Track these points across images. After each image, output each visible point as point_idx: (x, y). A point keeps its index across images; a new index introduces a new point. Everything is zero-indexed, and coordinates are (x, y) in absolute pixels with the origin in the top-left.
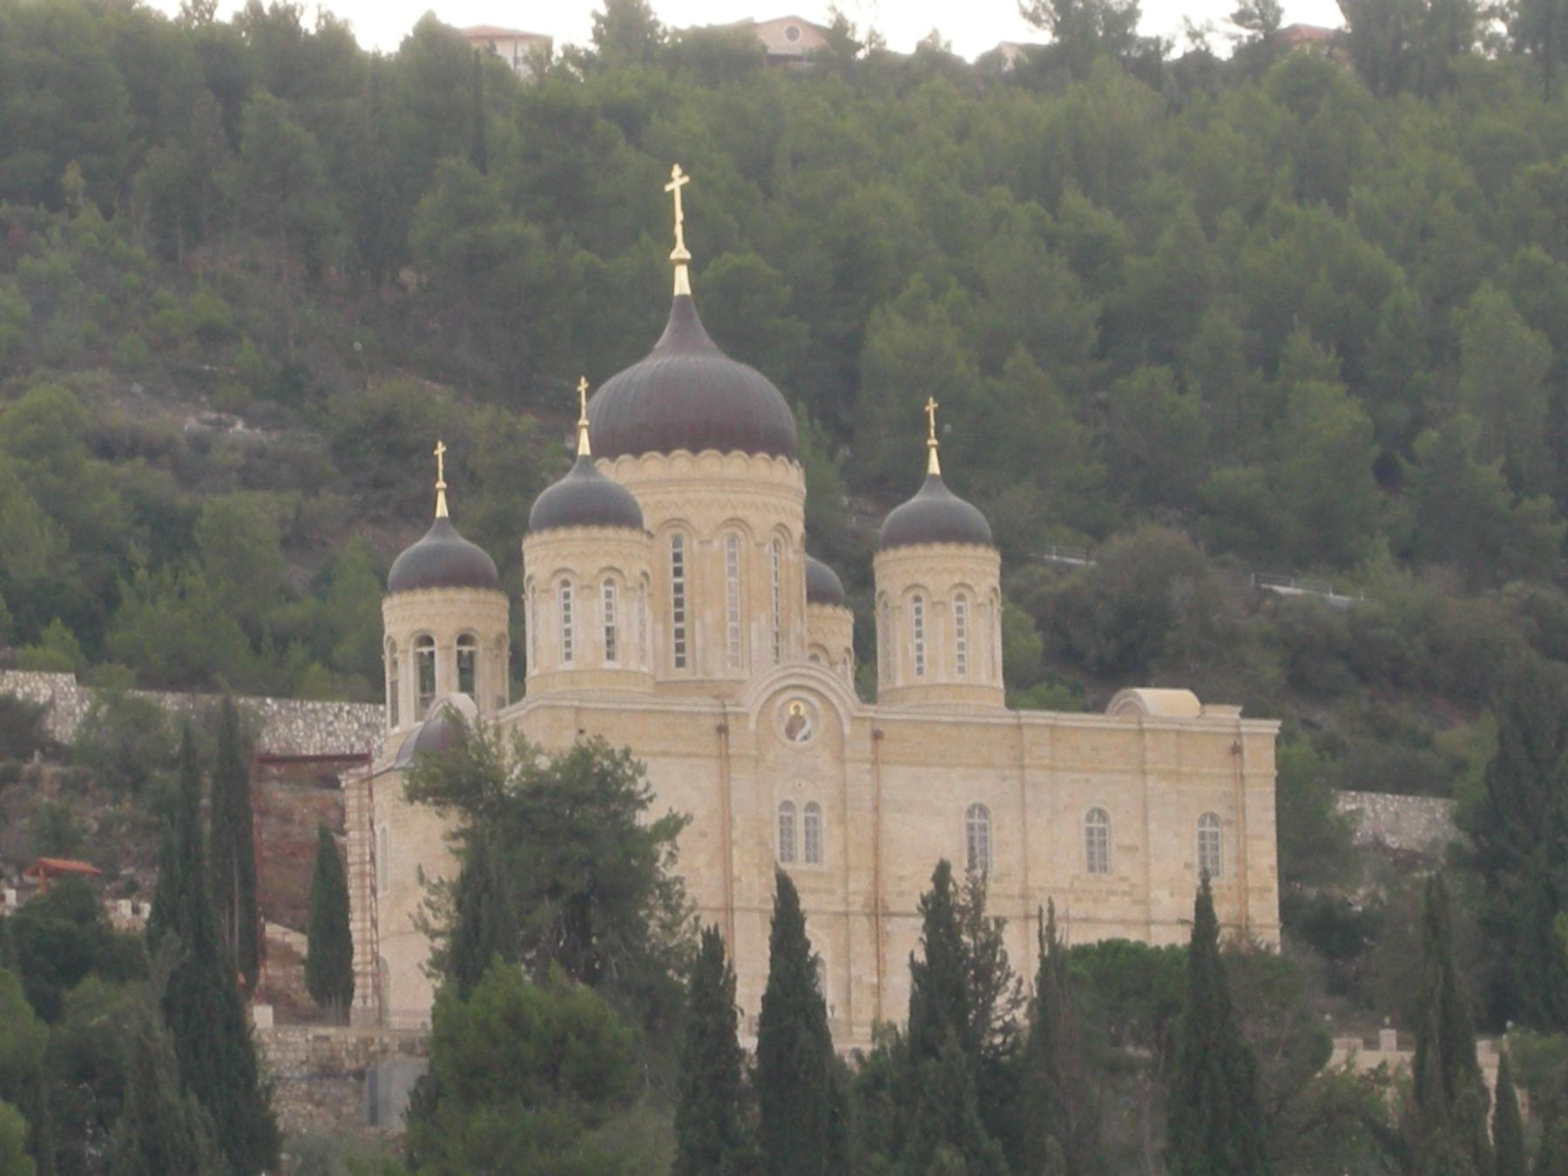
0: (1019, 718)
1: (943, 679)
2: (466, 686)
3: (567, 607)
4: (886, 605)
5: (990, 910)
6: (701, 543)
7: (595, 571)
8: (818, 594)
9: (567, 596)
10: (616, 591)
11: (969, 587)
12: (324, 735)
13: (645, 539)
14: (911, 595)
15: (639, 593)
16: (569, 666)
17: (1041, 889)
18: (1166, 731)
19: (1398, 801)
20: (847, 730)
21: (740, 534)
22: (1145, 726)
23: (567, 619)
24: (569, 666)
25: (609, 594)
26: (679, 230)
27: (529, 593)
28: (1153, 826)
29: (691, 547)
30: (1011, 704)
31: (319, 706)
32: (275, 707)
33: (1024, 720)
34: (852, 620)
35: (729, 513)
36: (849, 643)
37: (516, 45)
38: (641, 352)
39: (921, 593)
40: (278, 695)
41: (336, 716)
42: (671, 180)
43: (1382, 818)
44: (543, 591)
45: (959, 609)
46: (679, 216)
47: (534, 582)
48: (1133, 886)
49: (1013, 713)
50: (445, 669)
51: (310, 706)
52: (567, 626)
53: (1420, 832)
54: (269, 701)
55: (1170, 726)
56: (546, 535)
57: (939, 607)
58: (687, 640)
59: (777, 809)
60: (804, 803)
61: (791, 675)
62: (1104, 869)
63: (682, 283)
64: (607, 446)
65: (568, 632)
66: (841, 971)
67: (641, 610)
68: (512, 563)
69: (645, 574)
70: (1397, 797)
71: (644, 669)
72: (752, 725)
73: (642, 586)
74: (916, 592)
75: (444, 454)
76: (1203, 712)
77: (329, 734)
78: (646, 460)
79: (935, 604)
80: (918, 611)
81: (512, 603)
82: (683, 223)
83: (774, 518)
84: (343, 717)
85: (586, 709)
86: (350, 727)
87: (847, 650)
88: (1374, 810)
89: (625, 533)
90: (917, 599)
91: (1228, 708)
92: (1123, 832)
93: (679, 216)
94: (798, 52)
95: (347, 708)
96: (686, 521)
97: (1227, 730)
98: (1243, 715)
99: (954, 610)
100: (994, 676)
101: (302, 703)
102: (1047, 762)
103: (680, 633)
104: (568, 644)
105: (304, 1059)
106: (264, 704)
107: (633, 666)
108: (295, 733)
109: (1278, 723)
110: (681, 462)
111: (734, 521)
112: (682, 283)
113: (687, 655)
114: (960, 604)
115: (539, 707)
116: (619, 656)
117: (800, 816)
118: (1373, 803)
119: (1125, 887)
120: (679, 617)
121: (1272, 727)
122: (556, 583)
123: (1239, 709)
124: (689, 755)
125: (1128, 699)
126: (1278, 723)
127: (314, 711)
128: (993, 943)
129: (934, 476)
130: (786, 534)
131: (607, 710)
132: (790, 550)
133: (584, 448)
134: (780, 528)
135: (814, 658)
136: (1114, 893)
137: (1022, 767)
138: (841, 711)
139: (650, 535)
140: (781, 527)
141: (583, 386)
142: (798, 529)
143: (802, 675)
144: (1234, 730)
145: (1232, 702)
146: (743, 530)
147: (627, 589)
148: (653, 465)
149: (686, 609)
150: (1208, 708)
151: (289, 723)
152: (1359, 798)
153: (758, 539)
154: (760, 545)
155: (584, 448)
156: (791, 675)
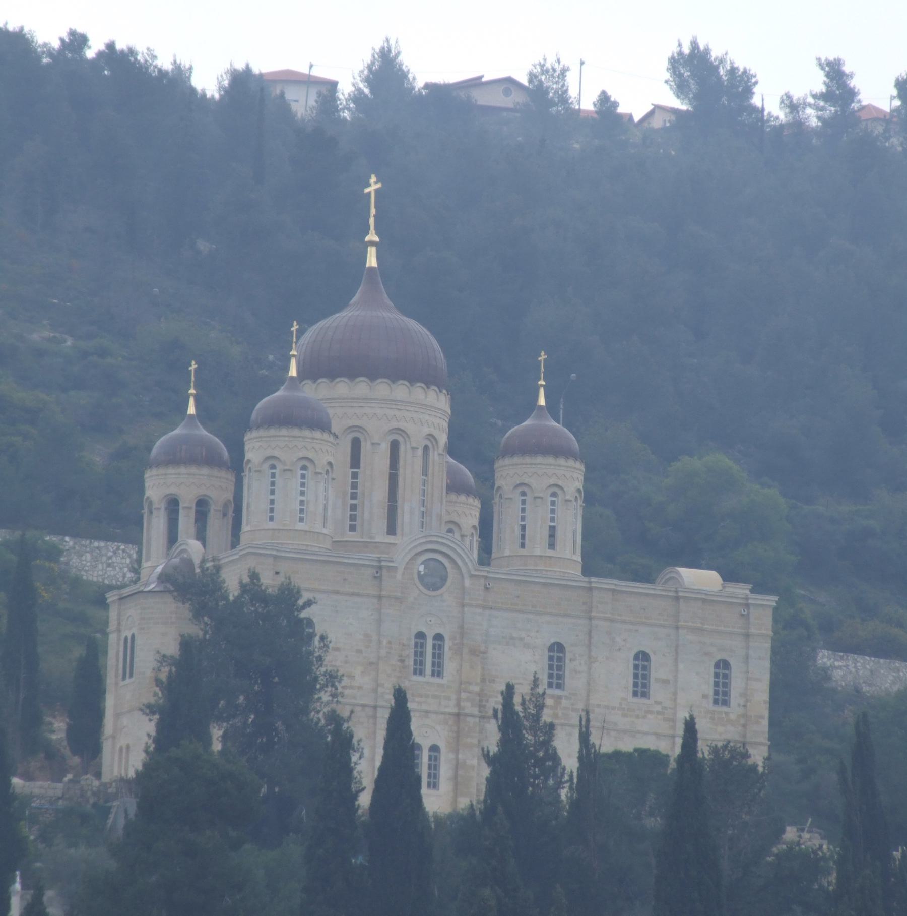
0: (590, 582)
1: (538, 552)
2: (201, 536)
3: (273, 484)
4: (501, 496)
5: (546, 717)
6: (373, 444)
7: (295, 459)
8: (455, 487)
9: (273, 476)
10: (309, 474)
11: (526, 485)
12: (105, 565)
13: (331, 439)
14: (520, 490)
15: (326, 477)
16: (271, 525)
17: (598, 706)
18: (696, 599)
19: (873, 661)
20: (467, 582)
21: (400, 439)
22: (681, 594)
23: (273, 492)
24: (271, 525)
25: (303, 476)
26: (372, 221)
27: (247, 472)
28: (681, 667)
29: (366, 447)
30: (587, 571)
31: (102, 544)
32: (71, 543)
33: (593, 585)
34: (480, 506)
35: (394, 424)
36: (476, 522)
37: (308, 87)
38: (341, 304)
39: (526, 489)
40: (74, 536)
41: (115, 553)
42: (369, 185)
43: (861, 673)
44: (256, 471)
45: (553, 503)
46: (373, 211)
47: (250, 465)
48: (665, 708)
49: (586, 579)
50: (186, 522)
51: (96, 544)
52: (272, 497)
53: (888, 685)
54: (67, 539)
55: (699, 596)
56: (262, 432)
57: (539, 500)
58: (358, 513)
59: (413, 637)
60: (433, 634)
61: (431, 542)
62: (645, 695)
63: (372, 261)
64: (310, 372)
65: (272, 502)
66: (452, 756)
67: (326, 490)
68: (237, 449)
69: (330, 464)
70: (873, 659)
71: (325, 531)
72: (399, 576)
73: (327, 472)
74: (523, 488)
75: (196, 370)
76: (724, 587)
77: (109, 565)
78: (337, 382)
79: (535, 498)
80: (524, 502)
81: (236, 480)
82: (375, 216)
83: (426, 430)
84: (119, 553)
85: (281, 557)
86: (124, 561)
87: (474, 527)
88: (855, 667)
89: (318, 434)
90: (273, 467)
91: (741, 585)
92: (658, 670)
93: (373, 211)
94: (511, 106)
95: (122, 547)
96: (364, 429)
97: (670, 594)
98: (752, 591)
99: (299, 476)
100: (574, 552)
101: (91, 542)
102: (609, 615)
103: (353, 507)
104: (272, 510)
105: (60, 795)
106: (63, 540)
107: (318, 528)
108: (84, 562)
109: (776, 598)
110: (362, 387)
111: (399, 430)
112: (372, 261)
113: (358, 523)
114: (304, 472)
115: (248, 554)
116: (558, 547)
117: (430, 643)
118: (855, 662)
119: (658, 708)
120: (354, 496)
121: (772, 600)
122: (266, 466)
123: (750, 586)
124: (353, 594)
125: (672, 575)
126: (776, 598)
127: (98, 548)
128: (546, 744)
129: (541, 407)
130: (361, 430)
131: (318, 560)
132: (436, 453)
133: (293, 372)
134: (431, 438)
135: (450, 531)
136: (651, 712)
137: (590, 619)
138: (464, 570)
139: (336, 436)
140: (431, 436)
141: (295, 327)
142: (443, 439)
143: (438, 543)
144: (588, 585)
145: (745, 581)
146: (403, 436)
147: (317, 473)
148: (342, 387)
149: (359, 491)
150: (728, 584)
151: (80, 555)
152: (845, 657)
153: (414, 445)
154: (414, 449)
155: (293, 372)
156: (431, 542)
